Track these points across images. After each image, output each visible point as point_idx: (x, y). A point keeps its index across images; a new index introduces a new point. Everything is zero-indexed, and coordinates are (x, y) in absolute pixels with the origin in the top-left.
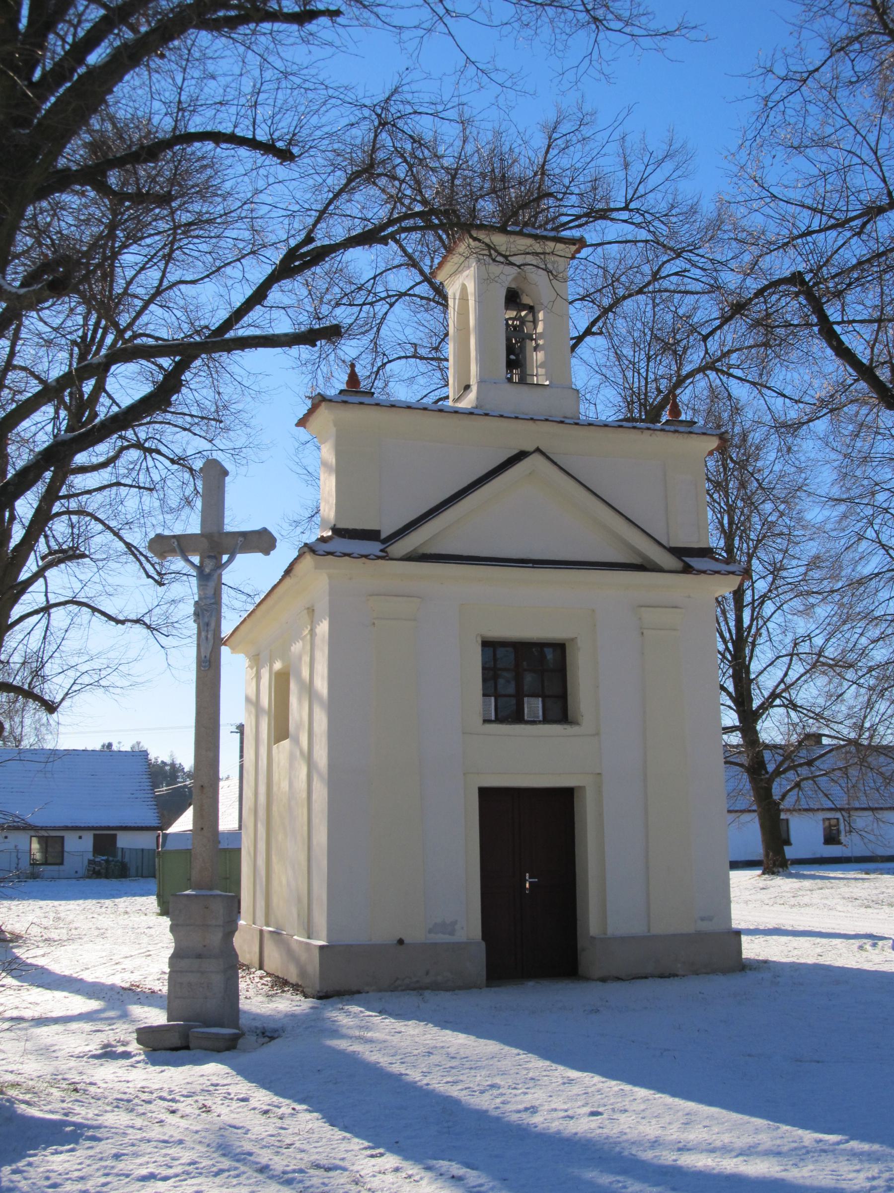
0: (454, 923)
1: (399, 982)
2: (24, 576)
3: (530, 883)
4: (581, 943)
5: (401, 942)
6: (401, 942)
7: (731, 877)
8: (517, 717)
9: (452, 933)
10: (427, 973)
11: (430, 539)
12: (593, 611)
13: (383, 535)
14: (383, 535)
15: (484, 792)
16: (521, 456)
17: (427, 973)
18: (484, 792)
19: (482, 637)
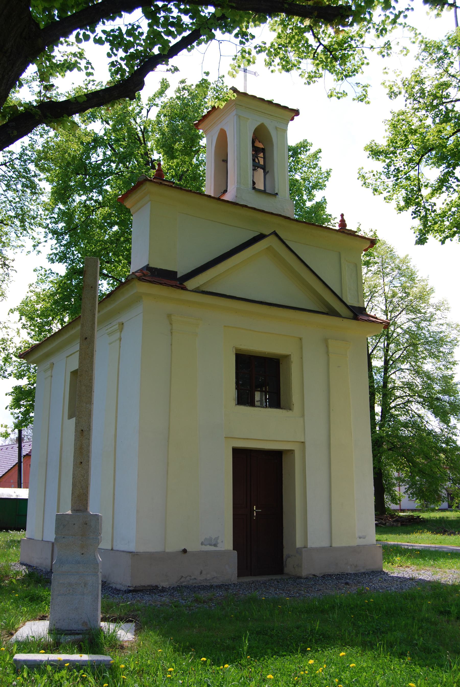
0: (217, 538)
1: (183, 579)
2: (101, 161)
3: (256, 512)
4: (285, 552)
5: (185, 551)
6: (185, 551)
7: (28, 495)
8: (252, 403)
9: (215, 545)
10: (201, 573)
11: (207, 282)
12: (301, 339)
13: (179, 275)
14: (179, 275)
15: (237, 452)
16: (260, 237)
17: (201, 573)
18: (237, 452)
19: (236, 350)
